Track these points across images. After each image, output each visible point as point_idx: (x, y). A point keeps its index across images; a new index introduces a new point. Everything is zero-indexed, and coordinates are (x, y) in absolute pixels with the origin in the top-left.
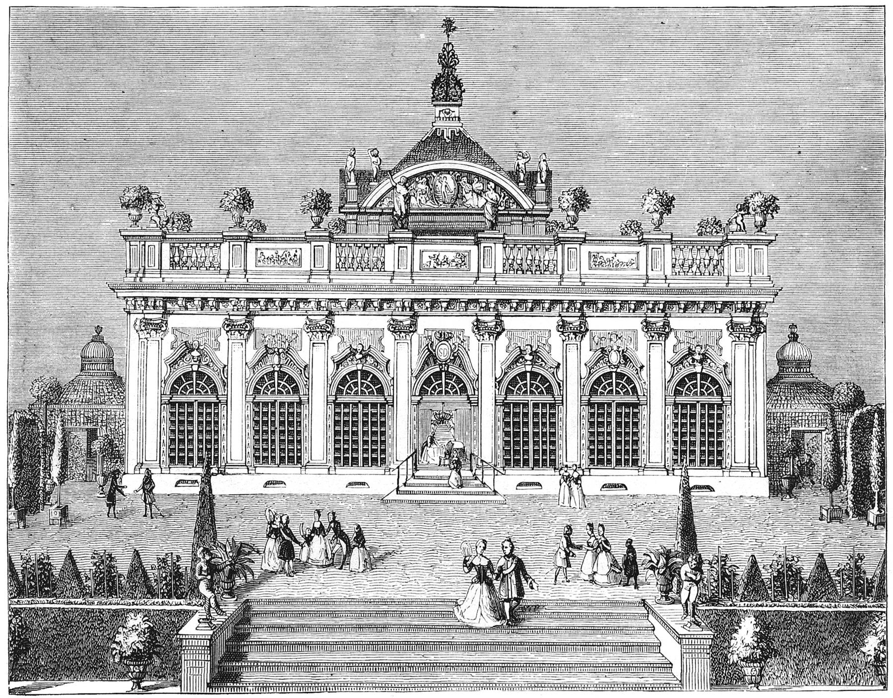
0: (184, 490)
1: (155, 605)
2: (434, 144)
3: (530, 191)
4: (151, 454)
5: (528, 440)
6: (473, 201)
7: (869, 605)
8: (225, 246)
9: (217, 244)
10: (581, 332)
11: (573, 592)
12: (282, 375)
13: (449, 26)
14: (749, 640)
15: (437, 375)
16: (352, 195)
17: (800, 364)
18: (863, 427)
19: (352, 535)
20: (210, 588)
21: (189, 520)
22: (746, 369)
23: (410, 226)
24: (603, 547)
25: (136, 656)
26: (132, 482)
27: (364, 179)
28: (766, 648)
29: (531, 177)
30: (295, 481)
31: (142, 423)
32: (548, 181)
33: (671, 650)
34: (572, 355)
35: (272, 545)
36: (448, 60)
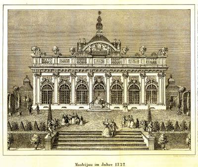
0: (45, 109)
1: (40, 133)
2: (96, 38)
3: (116, 48)
4: (38, 101)
5: (117, 97)
6: (104, 49)
7: (186, 131)
8: (53, 59)
9: (52, 58)
10: (127, 76)
11: (126, 129)
12: (66, 85)
13: (100, 13)
14: (162, 139)
15: (98, 85)
16: (80, 48)
17: (174, 82)
18: (186, 95)
19: (80, 118)
20: (51, 129)
21: (47, 114)
22: (161, 83)
23: (93, 55)
24: (132, 120)
25: (36, 143)
26: (34, 107)
27: (82, 45)
28: (166, 141)
29: (117, 44)
30: (69, 107)
31: (36, 96)
32: (120, 45)
33: (146, 141)
34: (108, 82)
35: (63, 120)
36: (99, 19)
